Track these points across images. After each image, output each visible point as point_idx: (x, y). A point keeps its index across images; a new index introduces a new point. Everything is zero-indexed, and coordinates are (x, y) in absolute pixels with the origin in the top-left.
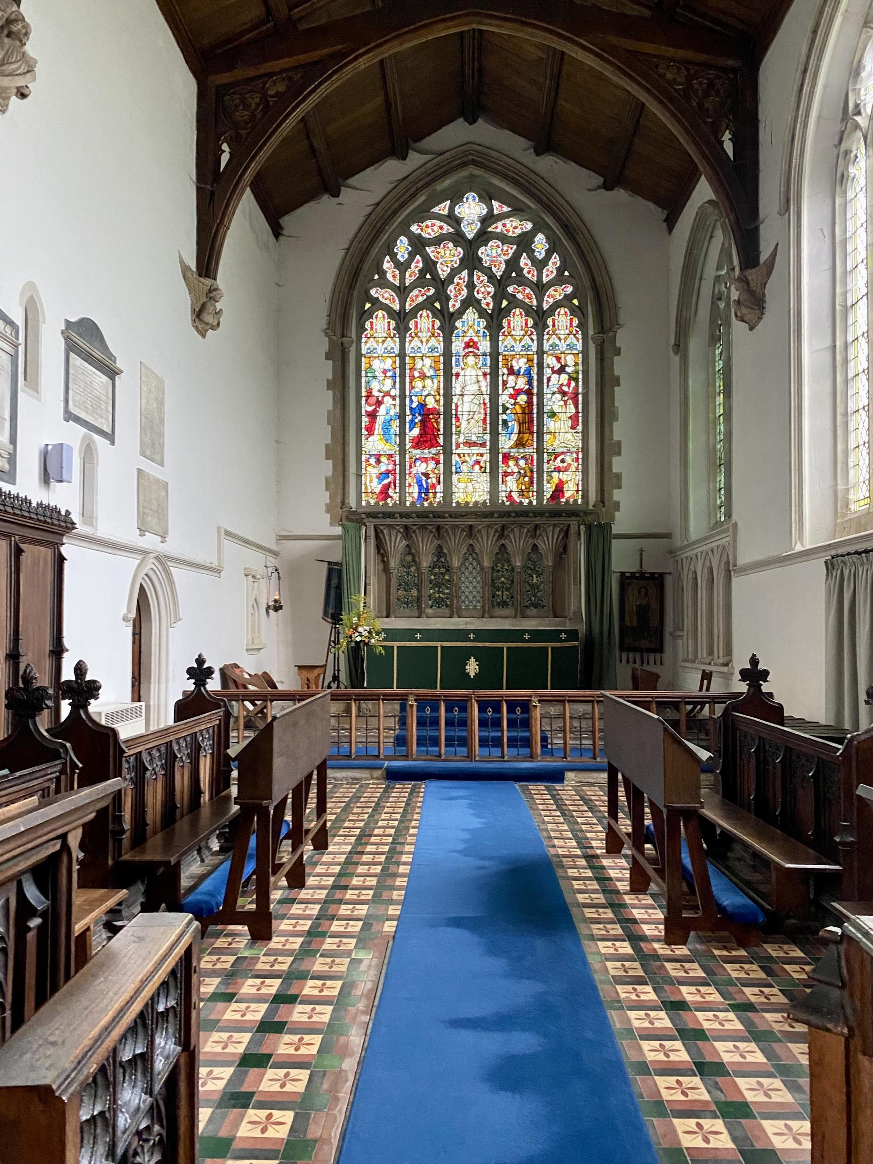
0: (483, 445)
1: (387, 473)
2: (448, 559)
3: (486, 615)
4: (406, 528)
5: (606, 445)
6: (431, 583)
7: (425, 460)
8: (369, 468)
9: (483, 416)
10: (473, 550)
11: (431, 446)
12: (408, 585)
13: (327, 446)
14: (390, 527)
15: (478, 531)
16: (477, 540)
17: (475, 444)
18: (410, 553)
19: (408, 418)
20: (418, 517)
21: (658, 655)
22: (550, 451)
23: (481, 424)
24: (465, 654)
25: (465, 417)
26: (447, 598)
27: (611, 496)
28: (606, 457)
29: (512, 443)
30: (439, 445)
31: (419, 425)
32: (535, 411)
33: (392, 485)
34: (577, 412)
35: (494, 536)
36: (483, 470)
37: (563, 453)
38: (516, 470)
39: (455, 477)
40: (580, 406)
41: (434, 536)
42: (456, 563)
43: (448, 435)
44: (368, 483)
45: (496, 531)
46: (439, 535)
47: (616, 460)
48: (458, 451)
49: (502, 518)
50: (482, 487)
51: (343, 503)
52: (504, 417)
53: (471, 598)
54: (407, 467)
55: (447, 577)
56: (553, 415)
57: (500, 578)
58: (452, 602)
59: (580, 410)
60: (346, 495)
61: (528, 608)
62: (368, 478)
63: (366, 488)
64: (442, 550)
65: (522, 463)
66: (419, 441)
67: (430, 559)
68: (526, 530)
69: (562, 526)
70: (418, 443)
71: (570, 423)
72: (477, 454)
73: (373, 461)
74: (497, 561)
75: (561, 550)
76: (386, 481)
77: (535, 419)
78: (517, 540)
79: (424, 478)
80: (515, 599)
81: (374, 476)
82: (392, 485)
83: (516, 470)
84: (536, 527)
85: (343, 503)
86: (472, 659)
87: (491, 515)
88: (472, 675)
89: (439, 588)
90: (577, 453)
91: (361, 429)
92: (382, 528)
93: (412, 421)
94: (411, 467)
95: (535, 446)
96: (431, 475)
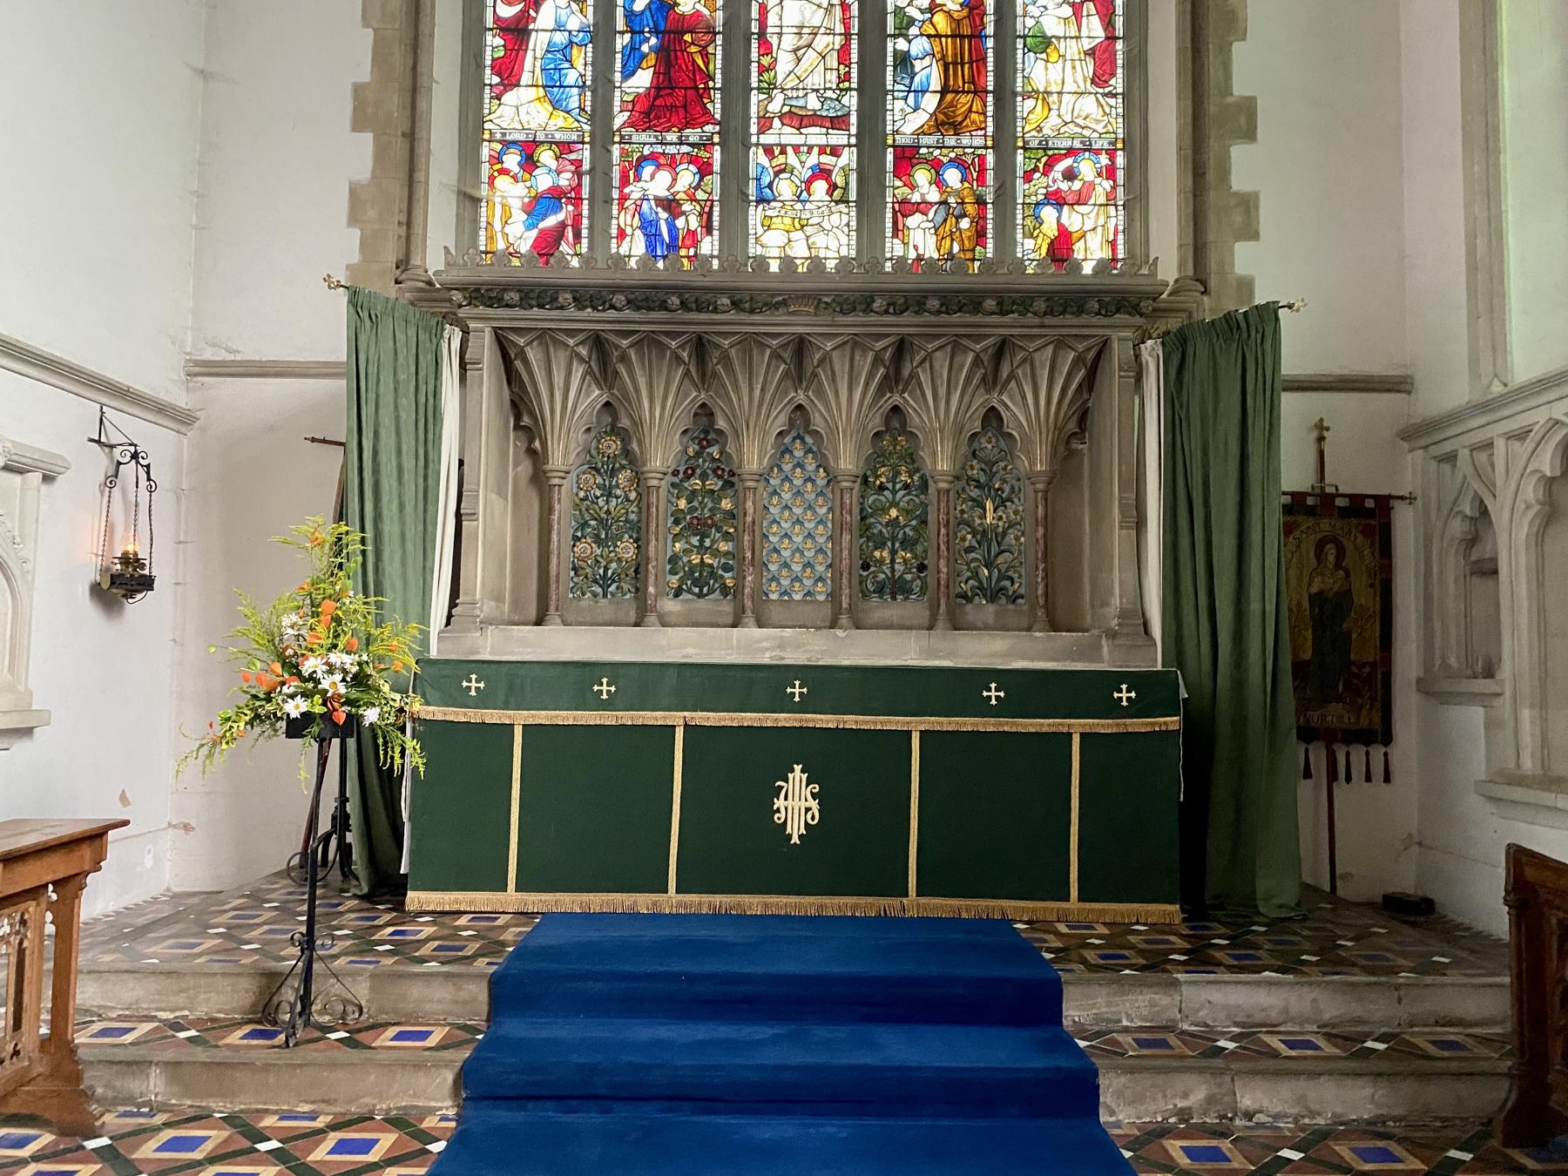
0: (838, 122)
1: (555, 196)
2: (731, 448)
3: (844, 619)
4: (598, 342)
5: (1212, 108)
6: (676, 522)
7: (672, 164)
8: (502, 182)
9: (839, 41)
10: (807, 422)
11: (690, 124)
12: (607, 528)
13: (358, 89)
14: (544, 336)
15: (822, 361)
16: (820, 392)
17: (814, 119)
18: (614, 430)
19: (622, 41)
20: (632, 304)
21: (1377, 752)
22: (1034, 144)
23: (833, 61)
24: (770, 756)
25: (789, 41)
26: (727, 568)
27: (1227, 263)
28: (1213, 145)
29: (920, 119)
30: (707, 118)
31: (652, 60)
32: (990, 30)
33: (569, 232)
34: (1111, 38)
35: (871, 376)
36: (837, 194)
37: (1071, 152)
38: (934, 195)
39: (755, 215)
40: (1119, 22)
41: (687, 373)
42: (753, 456)
43: (737, 91)
44: (497, 225)
45: (878, 360)
46: (703, 376)
47: (1239, 154)
48: (764, 139)
49: (901, 321)
50: (834, 245)
51: (403, 264)
52: (902, 44)
53: (797, 568)
54: (616, 183)
55: (726, 504)
56: (1043, 43)
57: (885, 511)
58: (739, 578)
59: (1119, 32)
60: (416, 240)
61: (969, 600)
62: (498, 209)
63: (491, 238)
64: (712, 421)
65: (952, 176)
66: (652, 106)
67: (677, 448)
68: (970, 357)
69: (1080, 347)
70: (650, 112)
71: (1090, 67)
72: (822, 150)
73: (512, 161)
74: (877, 458)
75: (1072, 426)
76: (551, 221)
77: (990, 53)
78: (942, 391)
79: (663, 215)
80: (929, 574)
81: (516, 205)
82: (569, 232)
83: (934, 195)
84: (1002, 349)
85: (403, 264)
86: (798, 774)
87: (862, 302)
88: (795, 830)
89: (703, 536)
90: (1111, 154)
91: (480, 66)
92: (521, 341)
93: (633, 48)
94: (625, 181)
95: (990, 130)
96: (686, 207)
